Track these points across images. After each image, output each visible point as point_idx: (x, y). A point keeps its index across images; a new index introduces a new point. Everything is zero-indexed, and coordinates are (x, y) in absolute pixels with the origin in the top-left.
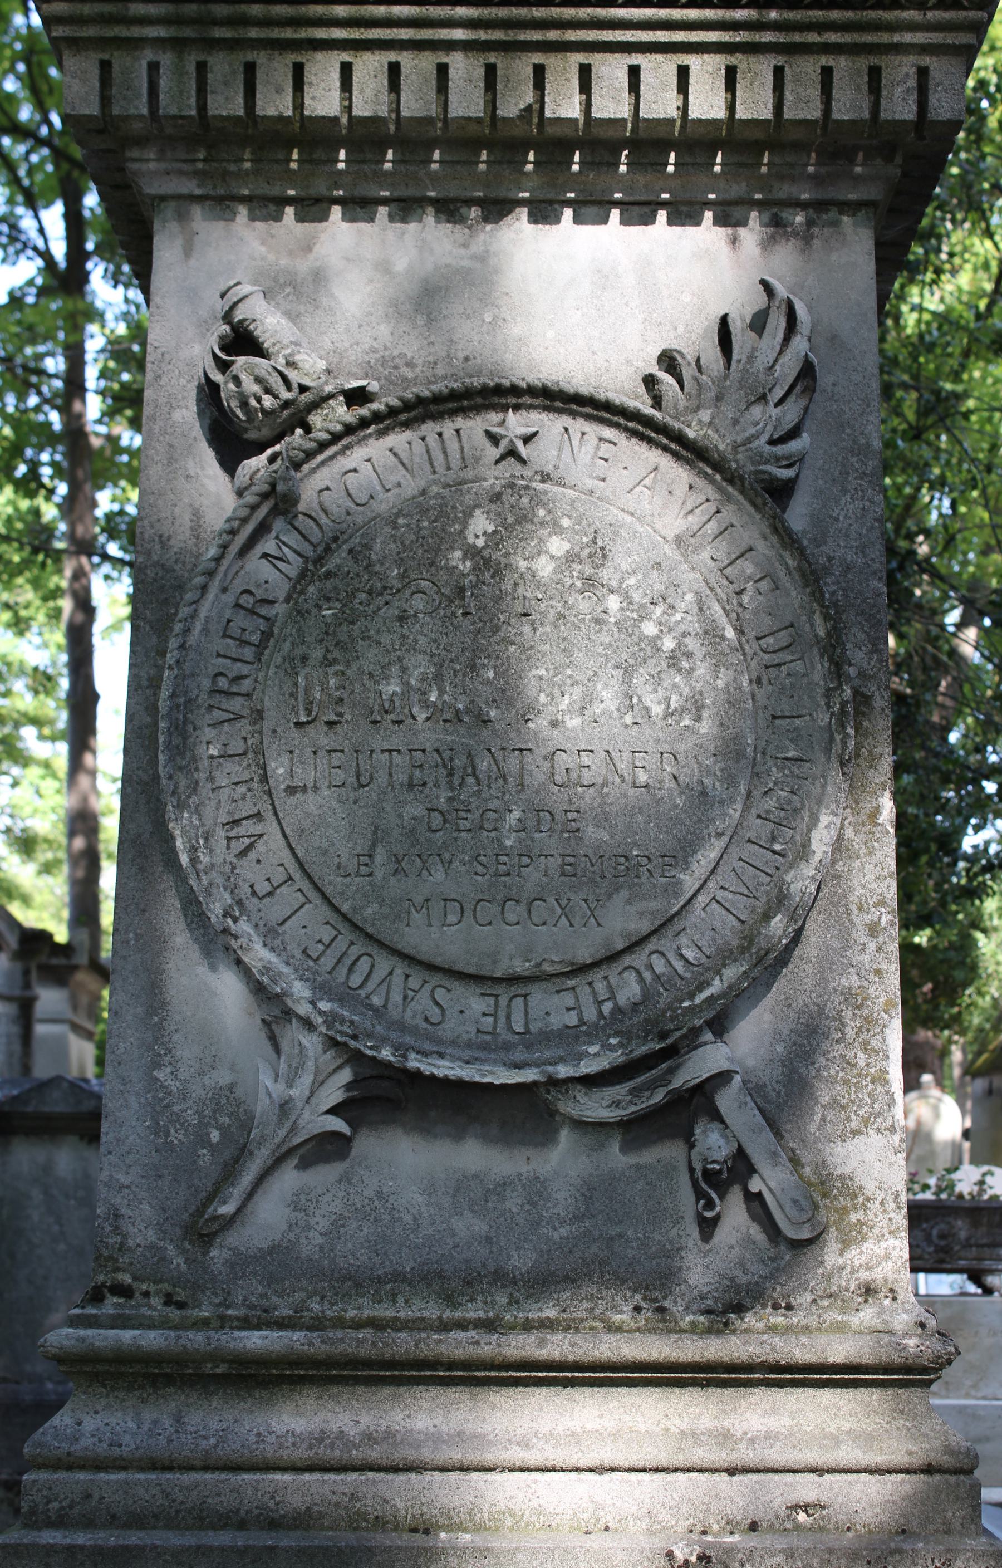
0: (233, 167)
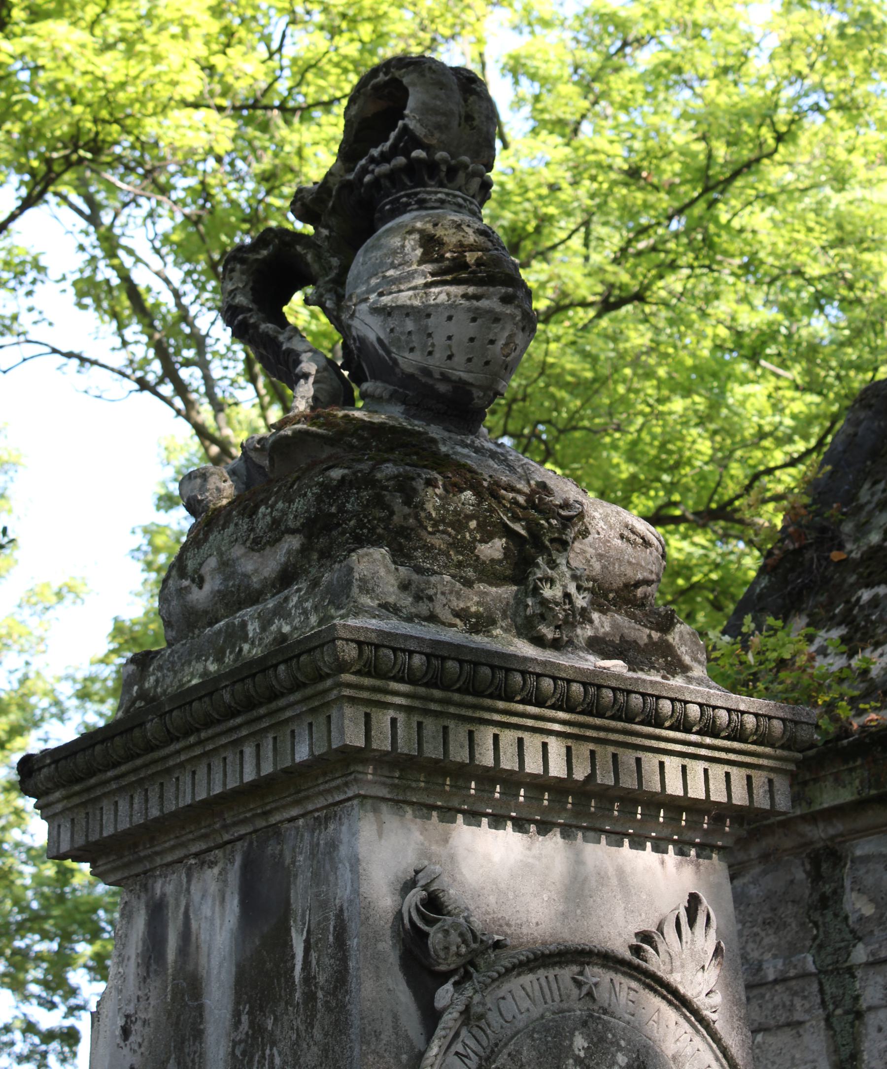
0: (414, 785)
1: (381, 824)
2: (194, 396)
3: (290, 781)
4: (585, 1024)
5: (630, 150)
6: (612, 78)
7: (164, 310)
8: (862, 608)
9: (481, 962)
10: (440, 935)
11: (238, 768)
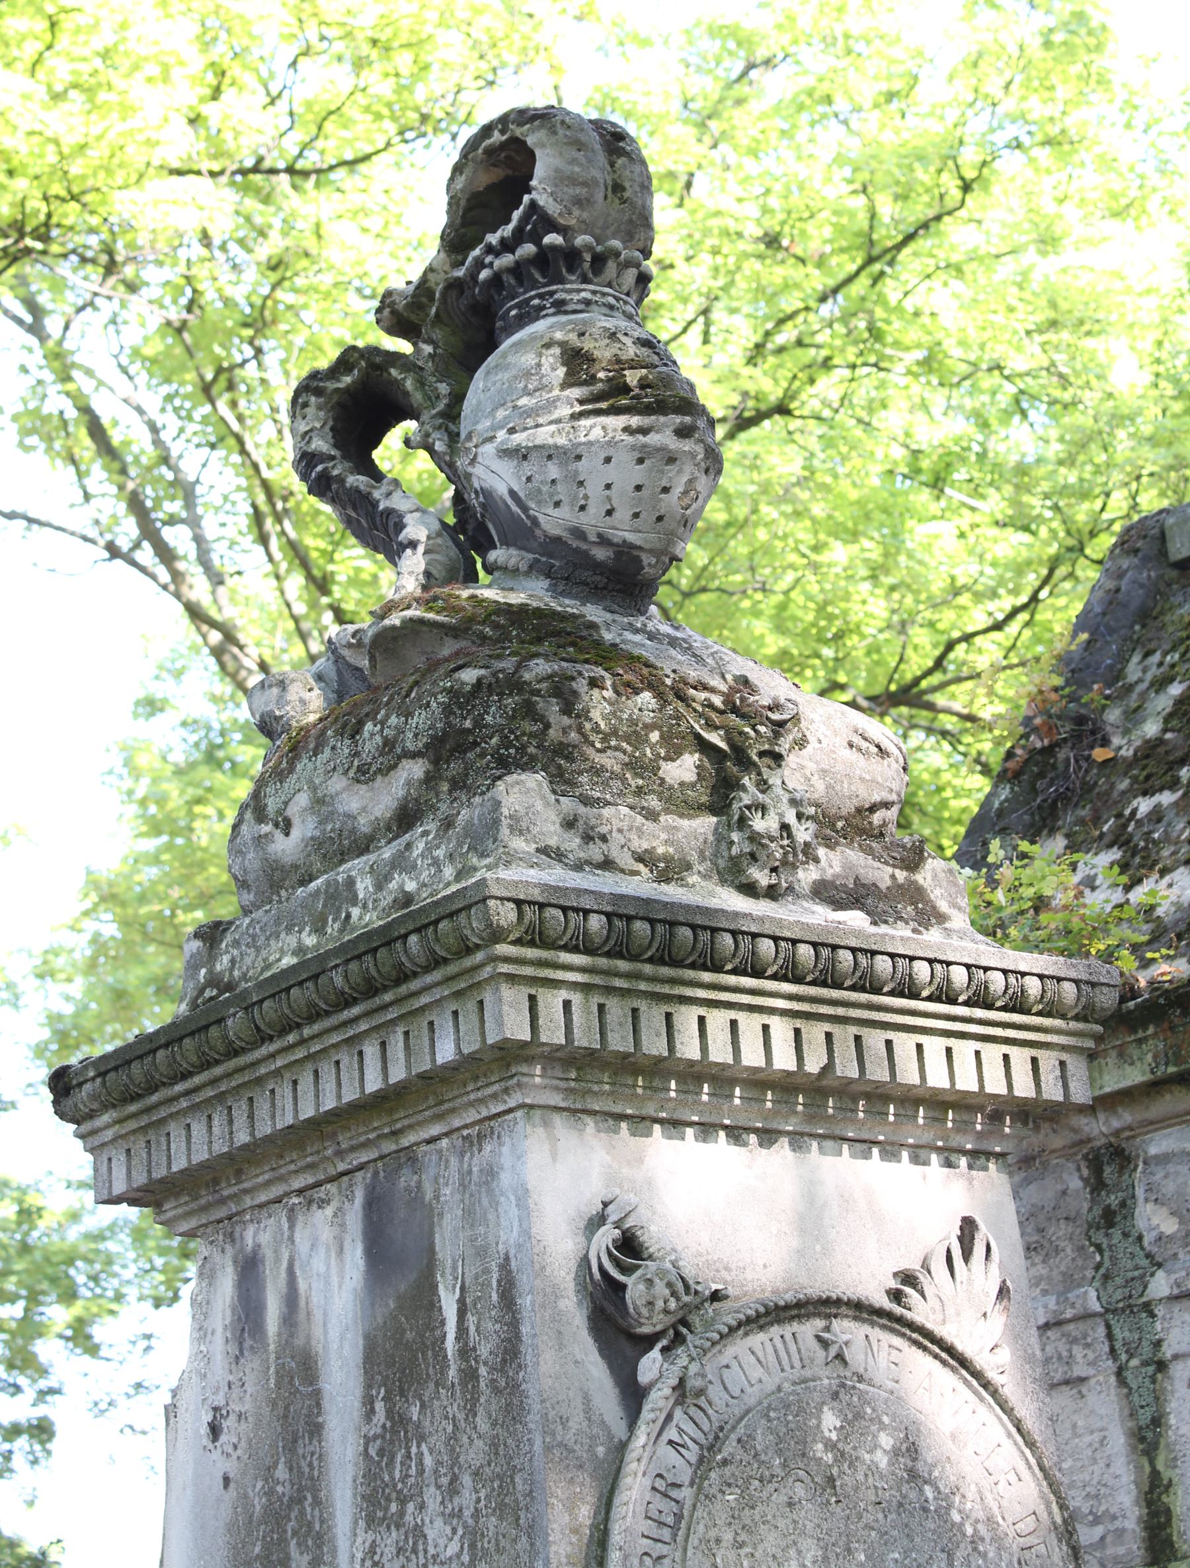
0: (596, 1088)
1: (554, 1141)
2: (181, 566)
3: (431, 1088)
4: (835, 1396)
5: (765, 210)
6: (737, 113)
7: (135, 449)
8: (1139, 823)
9: (695, 1320)
10: (642, 1287)
11: (356, 1074)
